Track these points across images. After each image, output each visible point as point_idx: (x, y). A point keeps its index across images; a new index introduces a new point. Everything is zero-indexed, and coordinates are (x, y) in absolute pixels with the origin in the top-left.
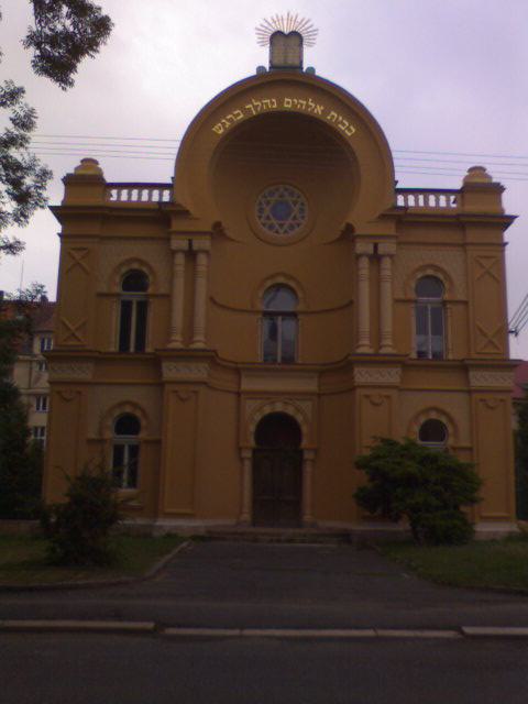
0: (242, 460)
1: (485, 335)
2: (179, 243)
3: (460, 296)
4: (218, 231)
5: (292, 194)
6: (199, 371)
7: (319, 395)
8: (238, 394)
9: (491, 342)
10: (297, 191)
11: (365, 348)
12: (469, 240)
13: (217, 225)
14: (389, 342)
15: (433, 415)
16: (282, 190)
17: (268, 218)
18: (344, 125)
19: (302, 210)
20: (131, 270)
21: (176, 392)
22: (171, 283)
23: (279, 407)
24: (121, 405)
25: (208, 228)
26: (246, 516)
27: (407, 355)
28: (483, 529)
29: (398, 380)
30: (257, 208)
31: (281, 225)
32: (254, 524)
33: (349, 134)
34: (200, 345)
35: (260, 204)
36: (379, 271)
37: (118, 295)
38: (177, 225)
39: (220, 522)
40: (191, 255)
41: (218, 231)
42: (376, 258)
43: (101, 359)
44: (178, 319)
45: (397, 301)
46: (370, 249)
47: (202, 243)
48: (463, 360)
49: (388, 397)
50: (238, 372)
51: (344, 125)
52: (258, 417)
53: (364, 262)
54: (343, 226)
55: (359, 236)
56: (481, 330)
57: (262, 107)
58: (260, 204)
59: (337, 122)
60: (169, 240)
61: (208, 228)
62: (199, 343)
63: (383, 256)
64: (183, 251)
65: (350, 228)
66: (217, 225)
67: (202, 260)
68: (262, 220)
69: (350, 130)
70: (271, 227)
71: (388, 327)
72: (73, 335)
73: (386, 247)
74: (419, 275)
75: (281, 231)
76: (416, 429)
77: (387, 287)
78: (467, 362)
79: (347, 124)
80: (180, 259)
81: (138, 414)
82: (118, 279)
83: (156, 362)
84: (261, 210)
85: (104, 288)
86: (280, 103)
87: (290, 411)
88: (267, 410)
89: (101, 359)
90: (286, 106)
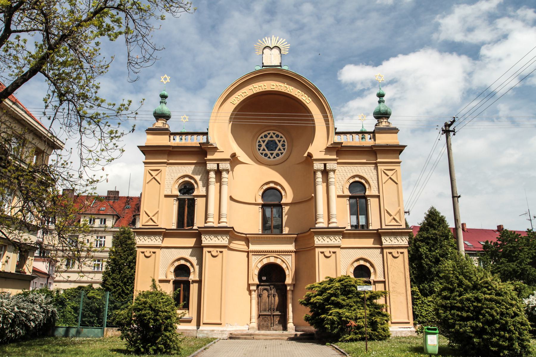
1: (390, 215)
5: (277, 136)
9: (394, 219)
10: (280, 135)
12: (379, 160)
15: (362, 263)
17: (264, 150)
19: (283, 145)
23: (272, 260)
34: (325, 225)
44: (212, 209)
53: (319, 175)
56: (388, 212)
61: (229, 157)
64: (214, 170)
68: (261, 151)
70: (266, 155)
84: (260, 146)
87: (279, 262)
88: (265, 261)
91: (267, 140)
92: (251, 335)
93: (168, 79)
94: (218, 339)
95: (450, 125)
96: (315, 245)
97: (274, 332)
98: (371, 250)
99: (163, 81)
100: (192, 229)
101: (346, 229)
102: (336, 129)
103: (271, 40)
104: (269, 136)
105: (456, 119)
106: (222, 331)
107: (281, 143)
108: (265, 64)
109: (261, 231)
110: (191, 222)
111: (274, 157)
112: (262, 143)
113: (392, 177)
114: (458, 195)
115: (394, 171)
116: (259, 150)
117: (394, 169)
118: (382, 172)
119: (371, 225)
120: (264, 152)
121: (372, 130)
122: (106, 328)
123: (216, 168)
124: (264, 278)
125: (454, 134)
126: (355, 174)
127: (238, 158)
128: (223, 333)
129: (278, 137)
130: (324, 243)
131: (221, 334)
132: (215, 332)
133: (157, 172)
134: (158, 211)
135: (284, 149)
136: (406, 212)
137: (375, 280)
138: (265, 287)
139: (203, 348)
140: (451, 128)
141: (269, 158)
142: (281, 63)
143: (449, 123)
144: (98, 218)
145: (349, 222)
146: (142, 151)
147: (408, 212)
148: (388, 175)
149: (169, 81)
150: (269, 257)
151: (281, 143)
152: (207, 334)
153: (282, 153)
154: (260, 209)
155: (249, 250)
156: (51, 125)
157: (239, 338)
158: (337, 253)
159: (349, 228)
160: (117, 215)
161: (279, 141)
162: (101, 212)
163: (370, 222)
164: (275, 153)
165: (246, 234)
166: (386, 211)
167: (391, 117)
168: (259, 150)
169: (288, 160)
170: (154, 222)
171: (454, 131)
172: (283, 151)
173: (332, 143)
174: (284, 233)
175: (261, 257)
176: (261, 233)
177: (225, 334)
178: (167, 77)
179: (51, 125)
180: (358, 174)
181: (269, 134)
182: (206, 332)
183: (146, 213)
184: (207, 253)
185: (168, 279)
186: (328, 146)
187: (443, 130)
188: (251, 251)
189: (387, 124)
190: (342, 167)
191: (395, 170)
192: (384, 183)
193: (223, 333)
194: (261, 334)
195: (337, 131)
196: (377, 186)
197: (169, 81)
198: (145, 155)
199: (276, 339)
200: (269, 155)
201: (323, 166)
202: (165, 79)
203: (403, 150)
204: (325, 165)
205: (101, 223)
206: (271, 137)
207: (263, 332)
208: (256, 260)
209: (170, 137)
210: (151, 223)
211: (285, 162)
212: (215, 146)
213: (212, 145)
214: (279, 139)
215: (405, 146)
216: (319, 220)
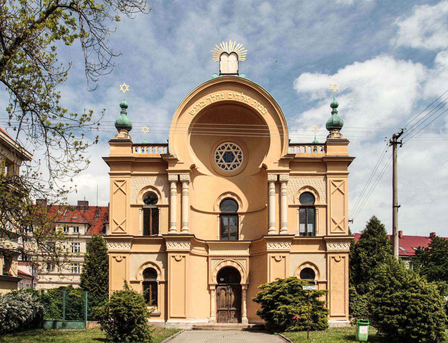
0: (210, 291)
1: (336, 224)
4: (193, 171)
6: (186, 247)
8: (208, 257)
9: (339, 227)
10: (237, 146)
11: (274, 230)
12: (328, 172)
15: (308, 266)
16: (229, 145)
19: (240, 157)
20: (144, 194)
23: (229, 264)
24: (147, 263)
25: (188, 168)
27: (294, 235)
28: (332, 322)
31: (229, 165)
34: (276, 233)
37: (141, 206)
41: (193, 171)
42: (278, 183)
43: (134, 241)
45: (290, 206)
46: (275, 178)
47: (185, 177)
53: (273, 186)
54: (260, 166)
56: (333, 221)
60: (167, 176)
61: (188, 168)
65: (264, 167)
68: (219, 163)
70: (223, 166)
73: (283, 177)
74: (302, 191)
75: (229, 169)
76: (299, 272)
77: (284, 198)
80: (174, 186)
82: (141, 196)
83: (163, 242)
84: (218, 157)
87: (235, 265)
88: (223, 265)
89: (134, 241)
92: (211, 326)
93: (127, 88)
94: (184, 330)
95: (397, 137)
96: (267, 251)
97: (231, 324)
99: (123, 90)
100: (157, 236)
101: (295, 236)
102: (290, 140)
103: (228, 45)
104: (226, 148)
105: (404, 131)
106: (186, 323)
107: (238, 154)
108: (222, 72)
109: (219, 238)
110: (156, 231)
111: (231, 169)
114: (398, 205)
118: (331, 183)
120: (222, 164)
121: (324, 142)
122: (87, 322)
124: (222, 279)
125: (401, 146)
126: (305, 185)
127: (197, 169)
128: (188, 325)
130: (275, 248)
131: (185, 326)
132: (181, 324)
133: (123, 183)
134: (125, 220)
137: (319, 281)
138: (223, 287)
139: (171, 337)
140: (399, 140)
141: (226, 169)
142: (238, 71)
143: (397, 135)
144: (72, 227)
145: (298, 230)
146: (107, 163)
147: (352, 221)
149: (128, 90)
150: (226, 261)
151: (238, 154)
152: (173, 326)
154: (218, 217)
155: (209, 255)
156: (17, 136)
157: (201, 329)
159: (298, 235)
160: (88, 224)
161: (236, 153)
162: (74, 221)
163: (317, 230)
164: (232, 164)
165: (206, 241)
166: (331, 220)
169: (244, 171)
171: (400, 143)
173: (286, 154)
174: (239, 240)
175: (219, 261)
176: (219, 240)
177: (189, 326)
178: (125, 85)
179: (17, 136)
180: (308, 185)
181: (226, 145)
182: (172, 324)
183: (115, 222)
184: (171, 257)
185: (138, 280)
187: (391, 142)
188: (210, 256)
189: (338, 136)
191: (343, 181)
193: (188, 325)
194: (220, 326)
195: (291, 142)
197: (121, 86)
199: (232, 330)
201: (277, 177)
202: (124, 88)
204: (278, 176)
205: (75, 231)
207: (221, 324)
208: (215, 264)
209: (132, 148)
210: (119, 231)
212: (175, 158)
213: (172, 156)
215: (353, 158)
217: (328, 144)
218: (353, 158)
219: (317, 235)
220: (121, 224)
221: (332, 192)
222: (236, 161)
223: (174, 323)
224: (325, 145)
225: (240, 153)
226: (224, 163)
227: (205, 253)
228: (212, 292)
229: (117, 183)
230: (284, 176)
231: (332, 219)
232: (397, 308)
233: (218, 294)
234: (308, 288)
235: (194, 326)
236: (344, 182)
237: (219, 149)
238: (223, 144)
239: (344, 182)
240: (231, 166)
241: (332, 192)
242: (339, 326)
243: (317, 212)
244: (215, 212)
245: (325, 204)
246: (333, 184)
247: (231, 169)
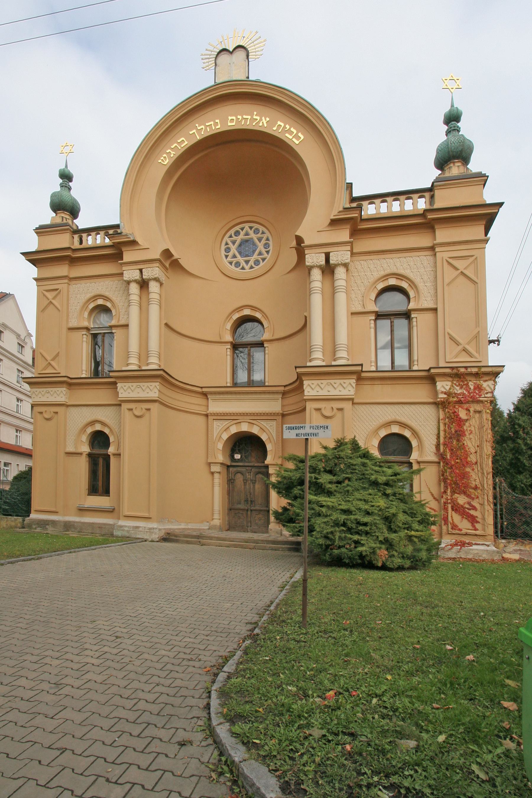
1: (458, 344)
2: (131, 274)
3: (428, 304)
5: (256, 231)
7: (283, 415)
9: (465, 350)
10: (261, 228)
12: (439, 240)
13: (167, 253)
14: (343, 354)
17: (234, 256)
18: (291, 133)
19: (266, 246)
21: (131, 410)
22: (128, 313)
23: (245, 428)
24: (388, 424)
26: (217, 522)
29: (352, 392)
30: (223, 247)
31: (247, 262)
32: (231, 528)
33: (297, 142)
35: (227, 244)
36: (333, 281)
38: (128, 256)
39: (190, 526)
40: (144, 284)
44: (134, 346)
48: (429, 370)
49: (341, 410)
50: (205, 395)
51: (291, 133)
52: (225, 436)
53: (317, 274)
55: (311, 246)
56: (452, 338)
57: (206, 129)
58: (227, 244)
59: (285, 131)
61: (157, 256)
62: (154, 363)
63: (336, 265)
66: (167, 253)
67: (154, 287)
68: (229, 259)
69: (298, 138)
70: (237, 264)
71: (342, 337)
72: (50, 364)
77: (341, 298)
78: (432, 371)
79: (295, 132)
80: (134, 288)
81: (107, 431)
84: (228, 250)
85: (74, 323)
86: (224, 121)
87: (255, 430)
88: (234, 430)
90: (230, 124)
91: (239, 239)
96: (305, 397)
98: (416, 406)
102: (350, 186)
104: (242, 233)
106: (150, 529)
107: (263, 241)
111: (252, 267)
112: (231, 245)
113: (466, 272)
115: (471, 259)
116: (227, 257)
117: (472, 256)
118: (445, 264)
119: (416, 363)
120: (235, 260)
121: (429, 186)
123: (323, 263)
124: (237, 456)
126: (388, 271)
128: (152, 532)
129: (258, 233)
130: (321, 393)
131: (148, 533)
132: (141, 529)
133: (55, 293)
134: (59, 353)
135: (268, 252)
136: (491, 342)
137: (420, 460)
138: (239, 469)
139: (69, 551)
141: (243, 268)
146: (31, 261)
147: (498, 341)
148: (456, 269)
150: (240, 422)
151: (263, 241)
152: (128, 531)
153: (263, 260)
154: (229, 350)
155: (208, 412)
158: (345, 411)
163: (415, 358)
164: (252, 259)
165: (202, 388)
167: (462, 118)
168: (227, 257)
170: (55, 369)
172: (265, 255)
173: (341, 209)
175: (227, 422)
176: (229, 385)
177: (155, 534)
180: (395, 271)
183: (42, 356)
184: (127, 411)
185: (79, 451)
186: (332, 217)
190: (362, 262)
191: (474, 258)
192: (448, 284)
193: (152, 532)
194: (215, 537)
196: (432, 292)
198: (35, 266)
199: (236, 546)
200: (243, 264)
201: (324, 259)
203: (496, 213)
206: (247, 234)
210: (50, 370)
211: (269, 273)
212: (132, 239)
214: (259, 235)
215: (500, 205)
216: (314, 356)
217: (436, 186)
218: (500, 205)
219: (415, 368)
220: (53, 359)
221: (447, 281)
222: (260, 254)
223: (129, 527)
224: (430, 190)
225: (268, 239)
226: (240, 259)
227: (202, 410)
228: (216, 476)
229: (47, 294)
230: (339, 253)
231: (449, 334)
232: (214, 688)
233: (230, 481)
234: (302, 431)
235: (168, 534)
236: (476, 258)
237: (231, 237)
238: (237, 228)
239: (476, 258)
240: (251, 263)
241: (447, 281)
242: (470, 556)
243: (415, 323)
244: (223, 340)
245: (432, 306)
246: (449, 263)
247: (252, 267)
